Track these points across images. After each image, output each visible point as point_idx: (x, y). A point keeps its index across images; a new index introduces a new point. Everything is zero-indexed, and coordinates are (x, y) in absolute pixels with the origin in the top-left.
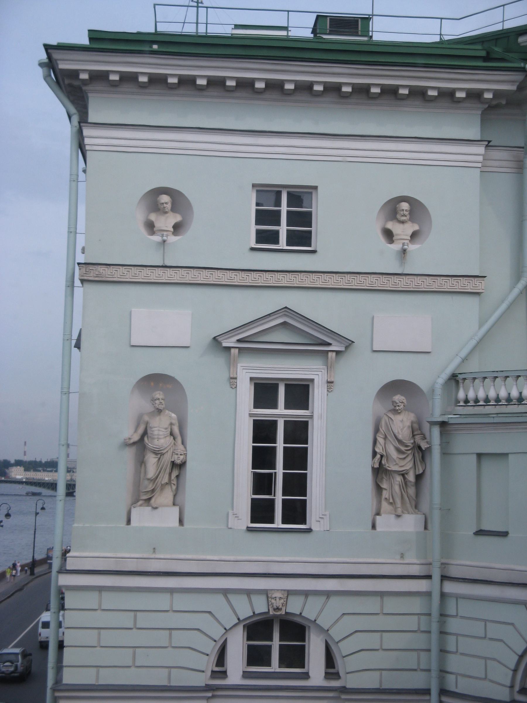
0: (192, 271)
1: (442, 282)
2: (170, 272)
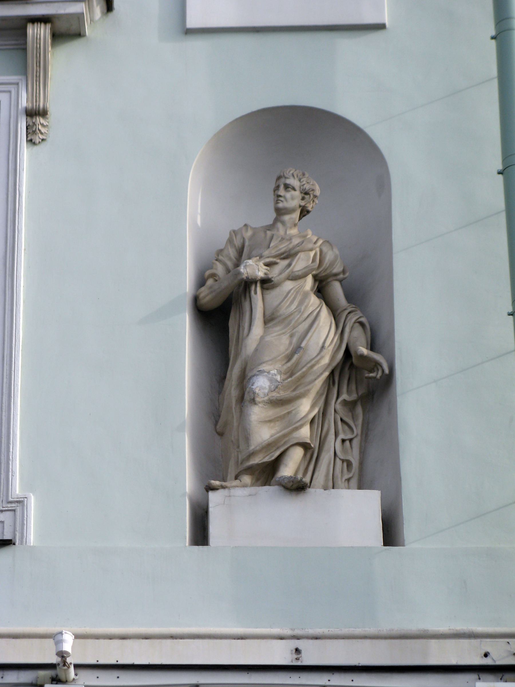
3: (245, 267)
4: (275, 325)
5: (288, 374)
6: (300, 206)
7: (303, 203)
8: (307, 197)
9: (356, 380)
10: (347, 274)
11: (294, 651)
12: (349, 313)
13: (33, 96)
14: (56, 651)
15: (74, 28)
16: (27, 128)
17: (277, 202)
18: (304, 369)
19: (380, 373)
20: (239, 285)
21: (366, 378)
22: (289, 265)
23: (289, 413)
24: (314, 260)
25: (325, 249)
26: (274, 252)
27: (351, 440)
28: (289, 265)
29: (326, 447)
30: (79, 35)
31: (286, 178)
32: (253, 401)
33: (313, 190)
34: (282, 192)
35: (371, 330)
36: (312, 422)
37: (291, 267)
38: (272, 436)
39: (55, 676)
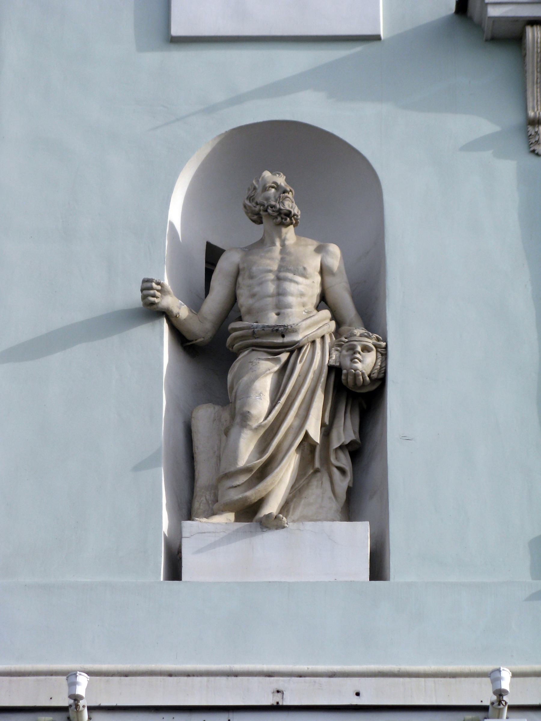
14: (68, 694)
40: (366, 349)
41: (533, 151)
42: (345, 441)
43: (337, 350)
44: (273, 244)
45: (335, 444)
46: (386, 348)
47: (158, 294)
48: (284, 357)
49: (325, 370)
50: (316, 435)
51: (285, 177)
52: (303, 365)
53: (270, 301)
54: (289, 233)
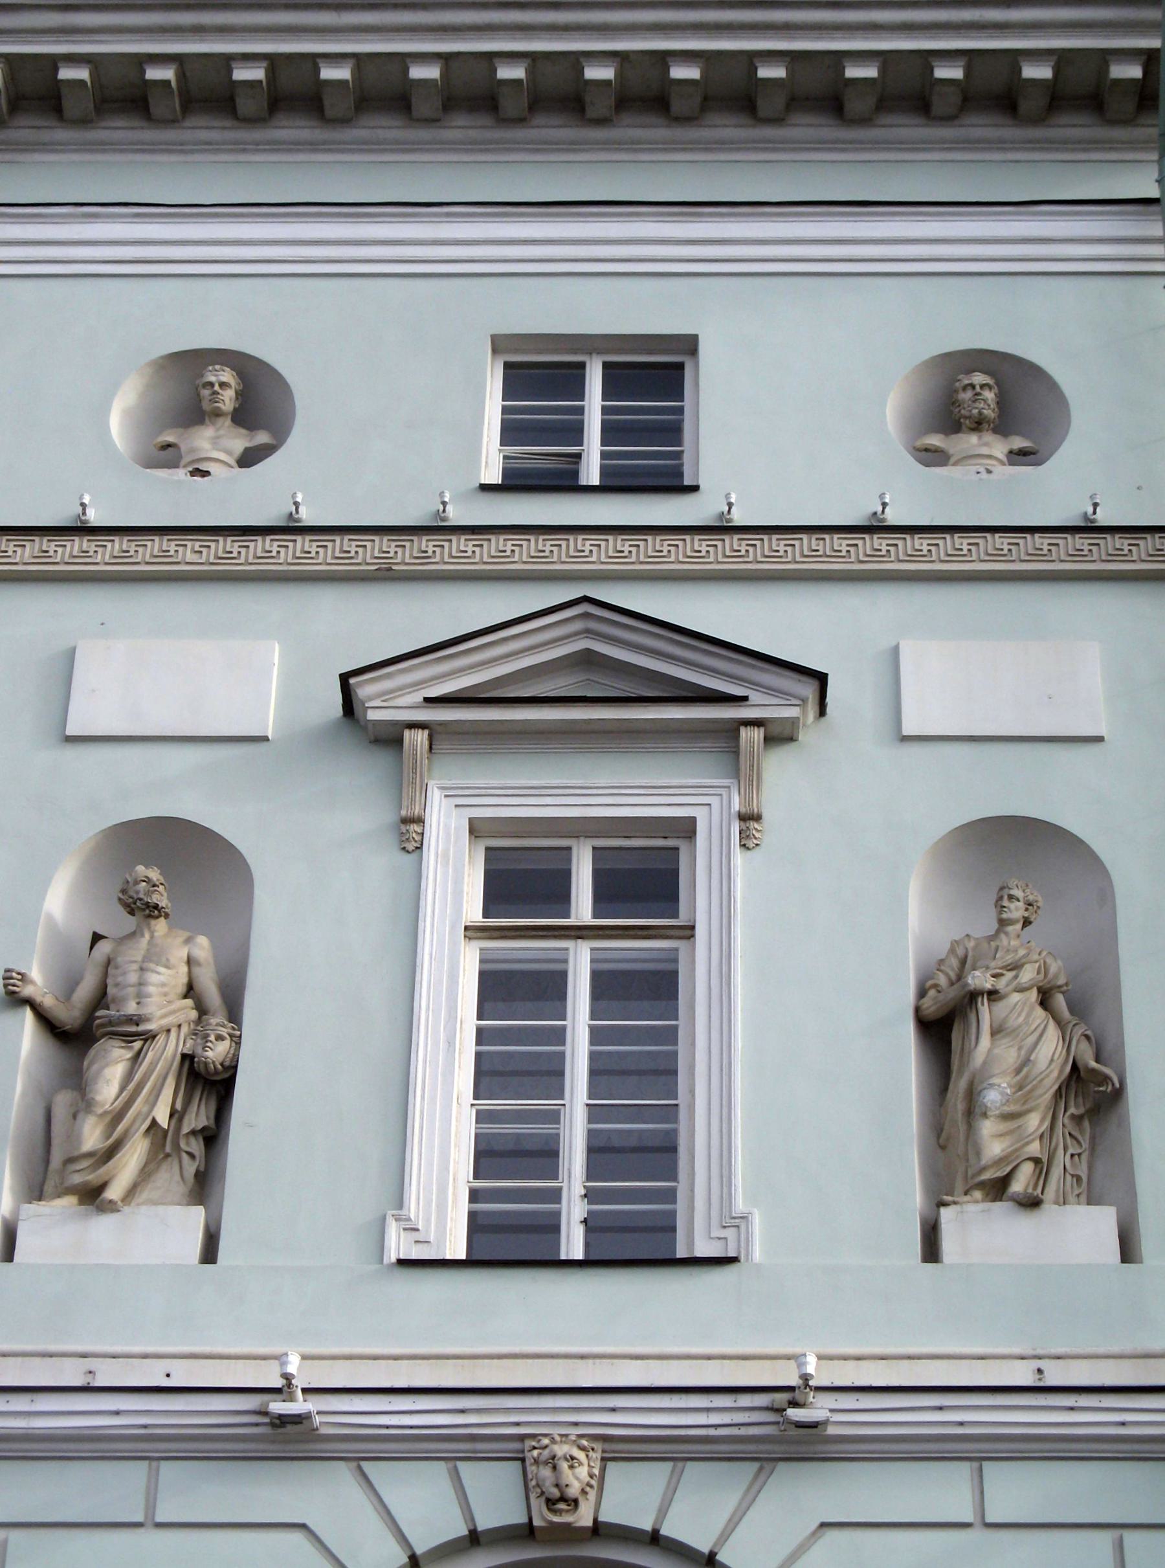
0: (533, 542)
1: (467, 546)
2: (497, 544)
3: (973, 978)
4: (1004, 1037)
5: (1017, 1088)
6: (1024, 917)
7: (1026, 914)
8: (1030, 908)
9: (1083, 1092)
10: (1070, 988)
11: (1036, 1371)
12: (1074, 1025)
13: (747, 799)
15: (787, 733)
16: (740, 833)
17: (1000, 913)
18: (1034, 1083)
19: (1110, 1088)
20: (964, 997)
21: (1095, 1092)
22: (1016, 977)
23: (1019, 1127)
24: (1038, 973)
25: (1048, 961)
26: (1000, 963)
27: (1079, 1155)
28: (1016, 977)
29: (1055, 1162)
30: (791, 739)
31: (1010, 889)
32: (985, 1115)
33: (1037, 901)
34: (1005, 903)
35: (1096, 1043)
36: (1041, 1136)
37: (1018, 979)
38: (1003, 1151)
39: (791, 1399)
40: (220, 1038)
41: (404, 848)
42: (196, 1126)
43: (192, 1039)
44: (143, 935)
45: (186, 1129)
46: (240, 1037)
47: (19, 983)
48: (137, 1045)
49: (178, 1058)
50: (163, 1120)
51: (159, 871)
52: (156, 1053)
53: (131, 990)
54: (160, 925)
